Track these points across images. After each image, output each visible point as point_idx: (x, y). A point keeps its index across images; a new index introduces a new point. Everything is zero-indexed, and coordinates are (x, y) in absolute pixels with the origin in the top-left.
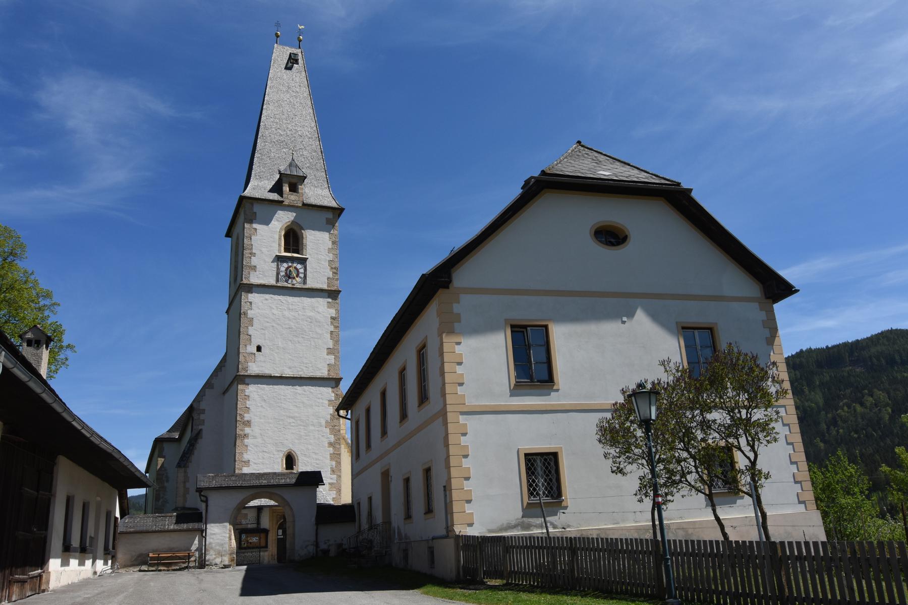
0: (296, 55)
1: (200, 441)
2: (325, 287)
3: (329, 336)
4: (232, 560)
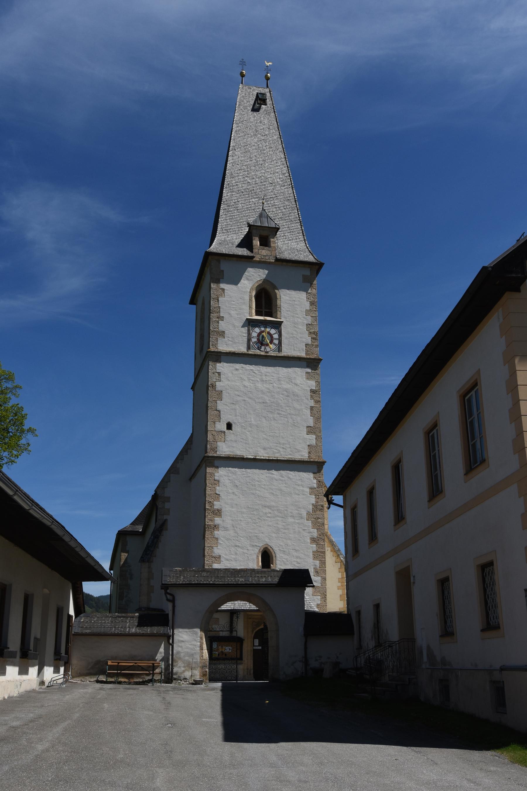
0: (264, 94)
2: (303, 355)
3: (308, 412)
4: (204, 675)
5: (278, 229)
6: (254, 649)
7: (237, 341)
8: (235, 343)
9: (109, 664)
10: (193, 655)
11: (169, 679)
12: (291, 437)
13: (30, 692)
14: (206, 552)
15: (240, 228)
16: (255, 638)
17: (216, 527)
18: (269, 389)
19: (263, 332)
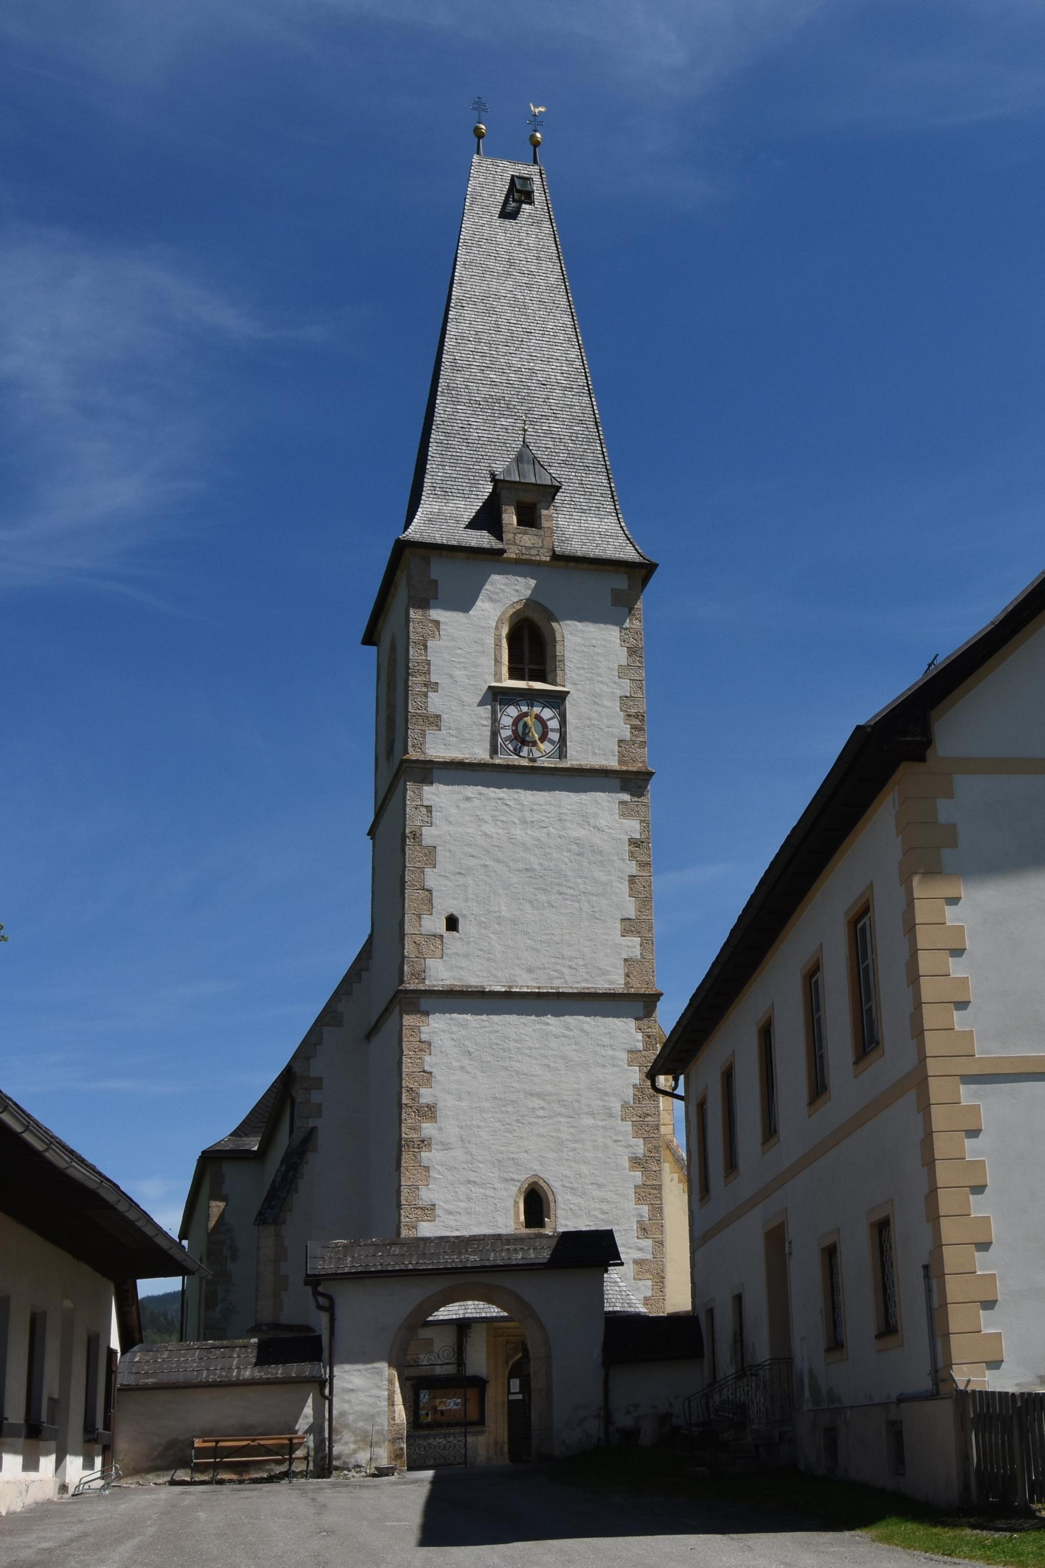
2: (613, 763)
3: (625, 887)
4: (398, 1456)
5: (557, 489)
6: (510, 1402)
7: (468, 736)
8: (465, 740)
9: (196, 1445)
10: (373, 1416)
11: (323, 1469)
12: (588, 943)
13: (43, 1504)
14: (403, 1198)
15: (474, 484)
16: (512, 1375)
17: (425, 1143)
18: (539, 840)
19: (526, 714)
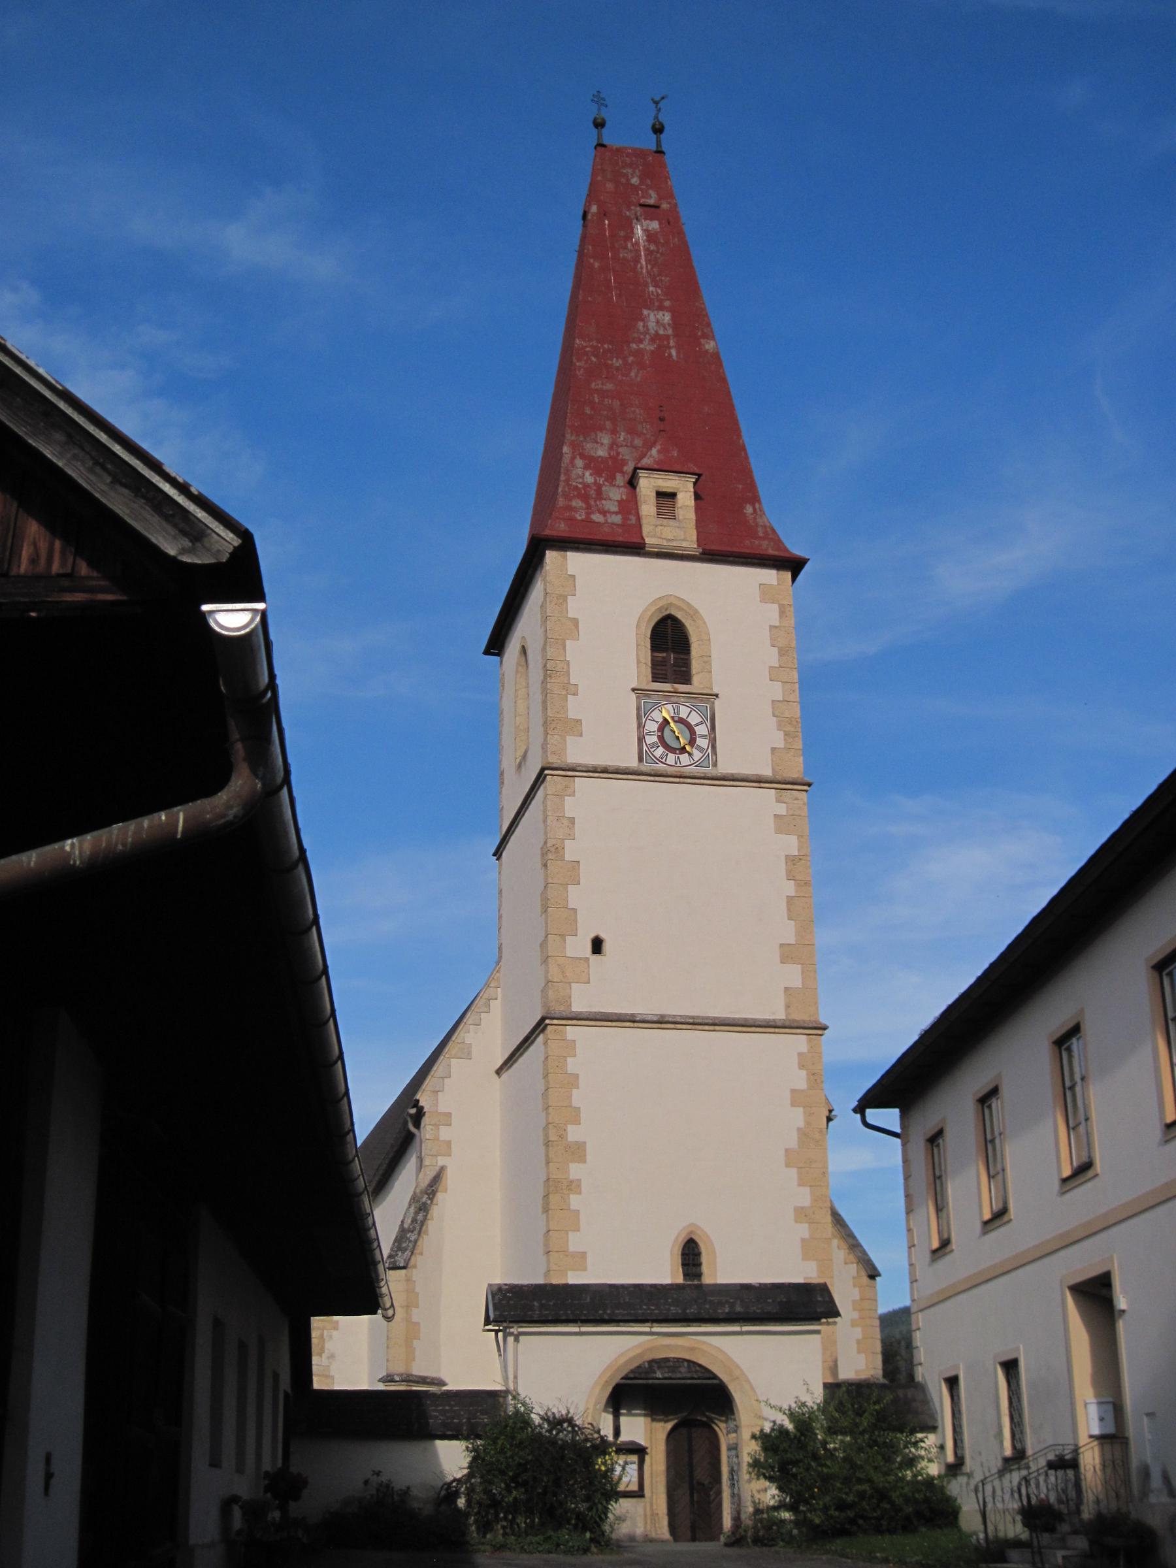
1: (440, 1196)
